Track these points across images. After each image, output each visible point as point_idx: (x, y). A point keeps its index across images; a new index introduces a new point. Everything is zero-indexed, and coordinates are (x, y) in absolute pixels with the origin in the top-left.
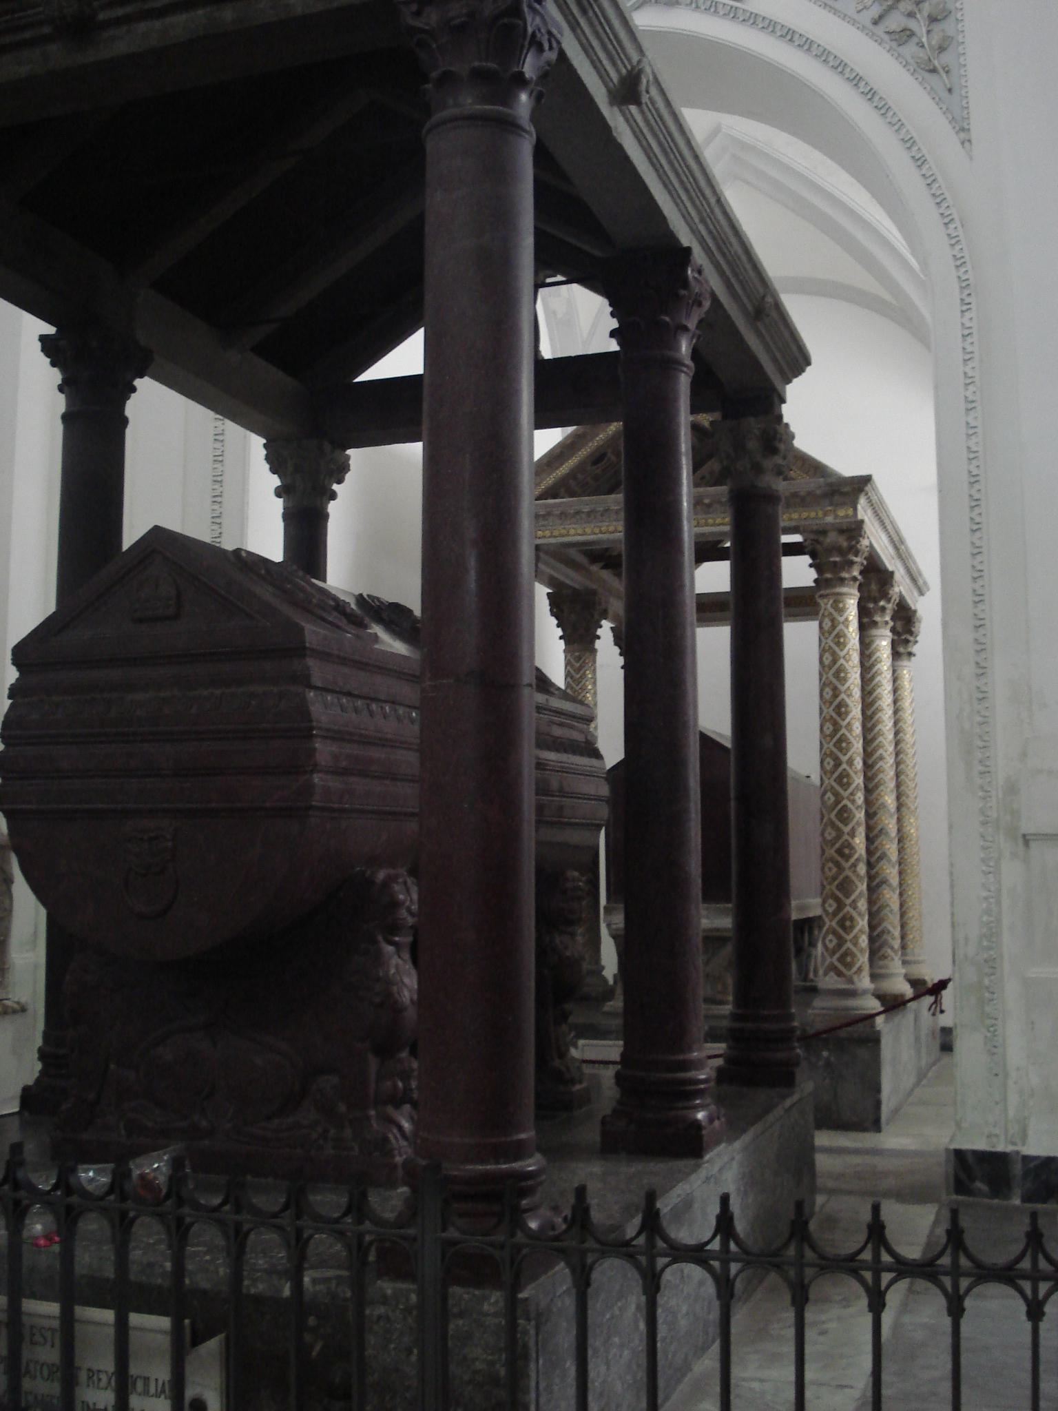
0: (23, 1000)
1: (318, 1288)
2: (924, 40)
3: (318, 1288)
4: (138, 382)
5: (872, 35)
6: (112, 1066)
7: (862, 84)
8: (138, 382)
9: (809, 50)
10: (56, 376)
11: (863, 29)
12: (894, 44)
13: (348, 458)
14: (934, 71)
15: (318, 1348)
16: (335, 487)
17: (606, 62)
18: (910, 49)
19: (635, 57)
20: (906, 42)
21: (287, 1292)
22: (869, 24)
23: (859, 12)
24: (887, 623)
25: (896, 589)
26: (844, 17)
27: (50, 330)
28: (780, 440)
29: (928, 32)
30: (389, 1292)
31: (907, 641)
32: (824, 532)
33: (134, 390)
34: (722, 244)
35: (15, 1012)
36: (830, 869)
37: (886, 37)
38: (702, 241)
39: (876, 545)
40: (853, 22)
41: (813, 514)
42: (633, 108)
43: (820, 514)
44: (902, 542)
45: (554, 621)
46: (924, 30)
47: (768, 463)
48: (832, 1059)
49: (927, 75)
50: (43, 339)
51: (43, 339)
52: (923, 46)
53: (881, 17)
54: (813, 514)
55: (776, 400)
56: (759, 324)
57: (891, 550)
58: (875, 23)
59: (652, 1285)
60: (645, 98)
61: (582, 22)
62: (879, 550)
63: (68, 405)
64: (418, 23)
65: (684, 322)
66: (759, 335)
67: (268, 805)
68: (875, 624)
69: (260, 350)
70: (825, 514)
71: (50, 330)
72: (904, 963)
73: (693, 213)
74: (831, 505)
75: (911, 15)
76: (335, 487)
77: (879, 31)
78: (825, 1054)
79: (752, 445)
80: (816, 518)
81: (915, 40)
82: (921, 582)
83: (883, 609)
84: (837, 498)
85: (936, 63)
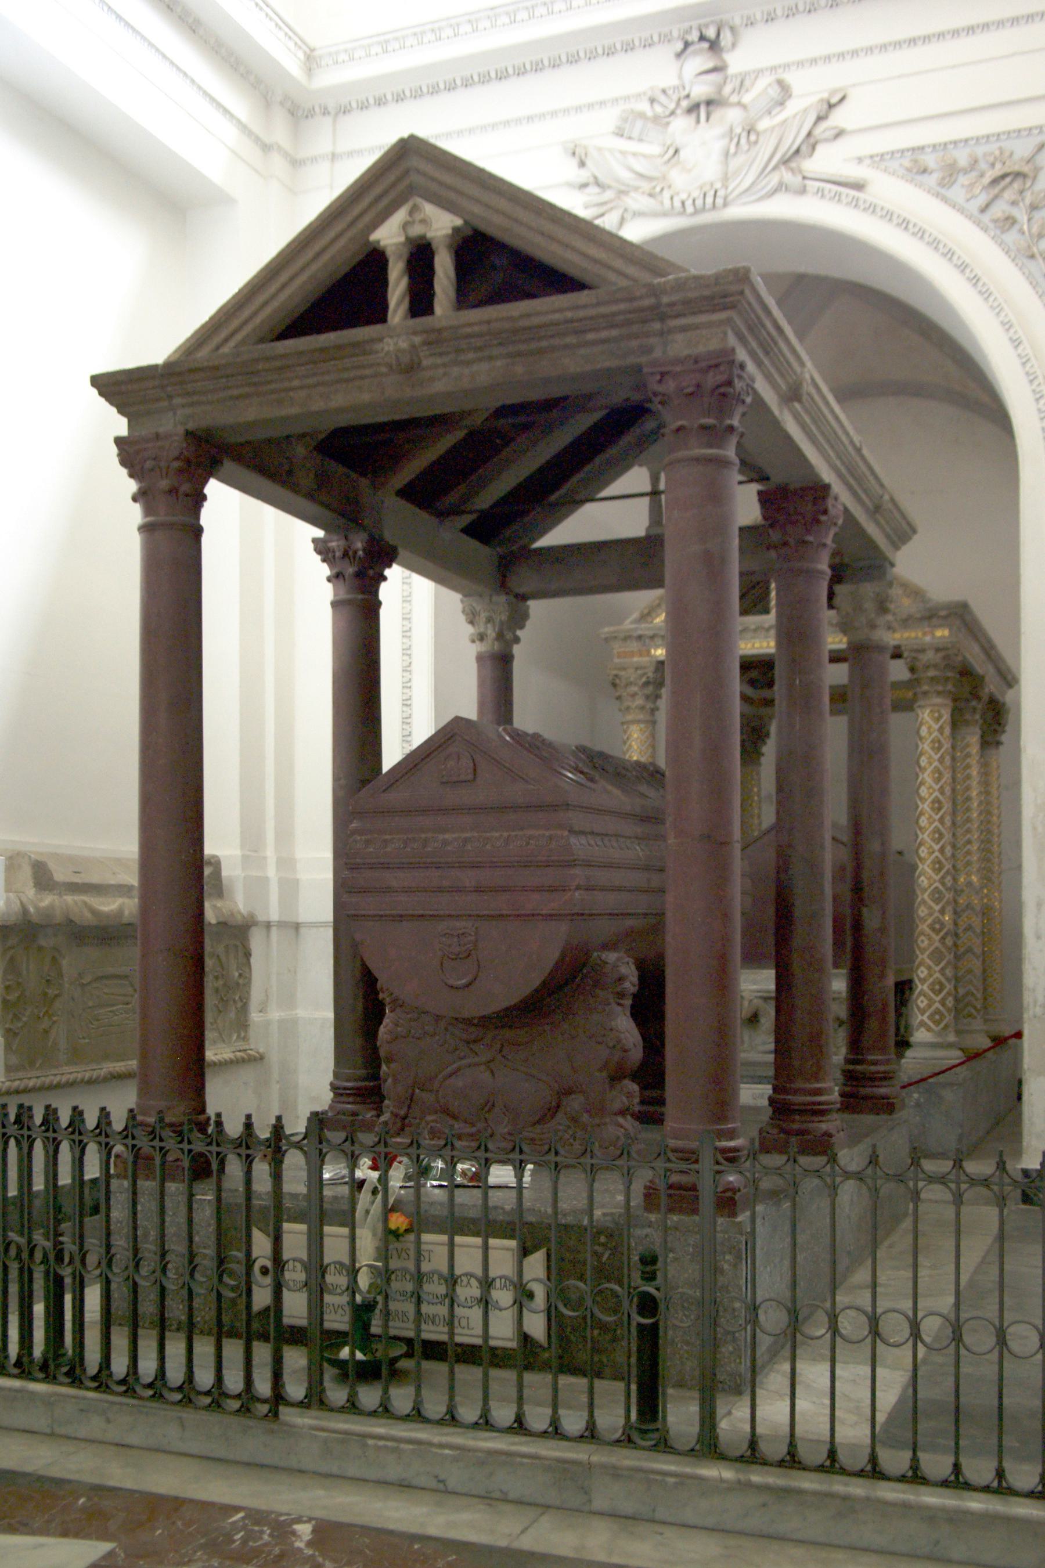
0: (261, 1050)
1: (607, 1218)
2: (1025, 227)
3: (607, 1218)
4: (387, 572)
5: (978, 223)
6: (417, 1091)
7: (968, 271)
8: (387, 572)
9: (922, 237)
11: (970, 217)
12: (998, 232)
13: (528, 607)
14: (1032, 257)
15: (606, 1255)
16: (519, 633)
17: (776, 376)
18: (1011, 237)
19: (798, 369)
20: (1008, 230)
21: (586, 1222)
22: (976, 213)
23: (968, 200)
24: (977, 721)
25: (987, 690)
26: (954, 206)
28: (891, 602)
29: (1029, 220)
30: (653, 1219)
31: (995, 731)
32: (923, 651)
33: (385, 579)
34: (852, 470)
35: (255, 1059)
36: (923, 941)
37: (991, 225)
38: (840, 475)
39: (968, 656)
40: (961, 210)
41: (913, 635)
42: (797, 405)
43: (920, 634)
44: (993, 647)
46: (1025, 218)
47: (882, 620)
48: (922, 1100)
49: (1025, 261)
52: (1023, 233)
53: (987, 206)
54: (913, 635)
55: (888, 565)
56: (878, 516)
57: (982, 657)
58: (983, 210)
59: (834, 1189)
60: (805, 398)
61: (766, 362)
62: (971, 660)
63: (335, 595)
64: (660, 389)
65: (824, 541)
66: (878, 524)
67: (544, 912)
68: (967, 723)
69: (466, 531)
70: (925, 634)
71: (320, 533)
72: (986, 1021)
73: (832, 454)
74: (929, 626)
75: (1014, 203)
76: (519, 633)
77: (986, 218)
78: (916, 1096)
79: (869, 605)
80: (916, 638)
81: (1017, 227)
82: (1009, 677)
83: (974, 709)
84: (935, 621)
85: (1035, 250)
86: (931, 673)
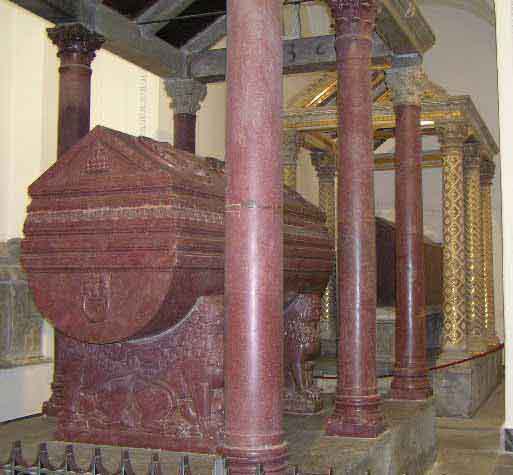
8: (97, 52)
10: (55, 49)
27: (52, 26)
45: (314, 168)
50: (48, 30)
51: (48, 30)
71: (52, 26)
86: (451, 136)
